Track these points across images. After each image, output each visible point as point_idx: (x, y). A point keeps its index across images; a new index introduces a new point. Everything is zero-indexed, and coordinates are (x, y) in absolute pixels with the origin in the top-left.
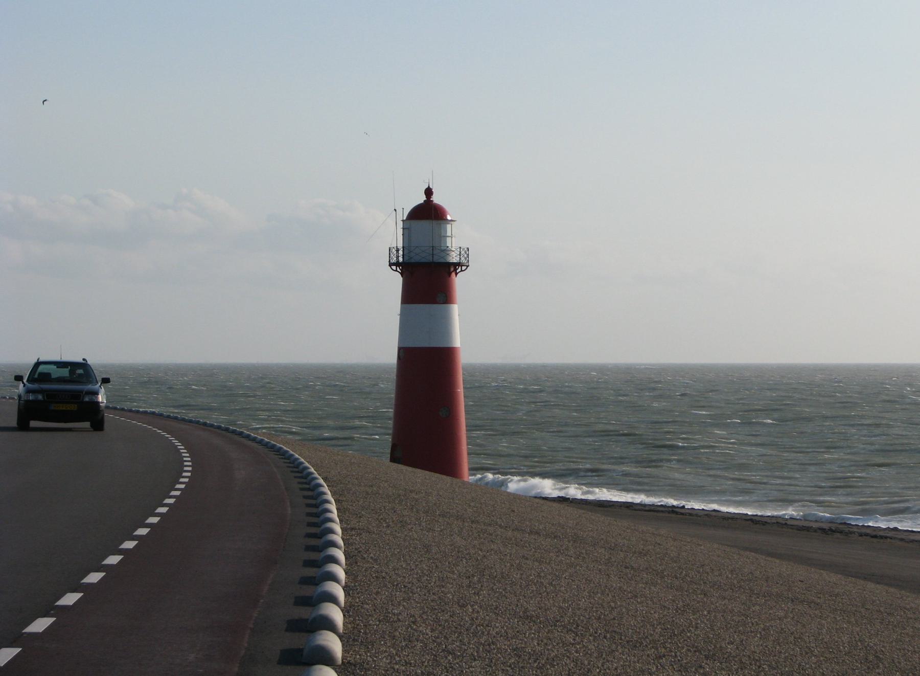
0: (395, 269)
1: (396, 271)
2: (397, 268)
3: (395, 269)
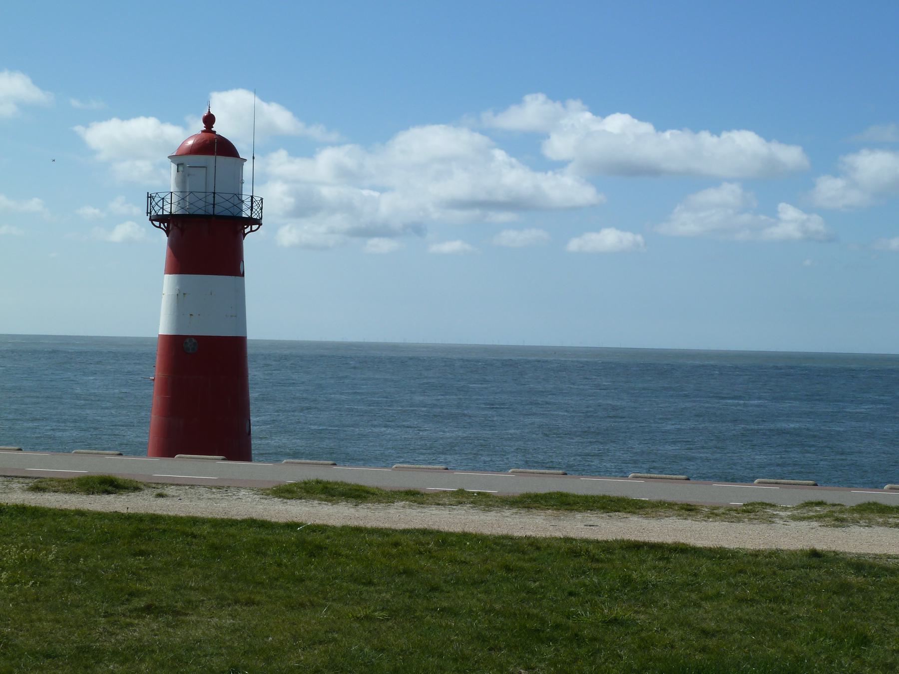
0: (158, 226)
1: (160, 227)
2: (160, 225)
3: (158, 226)
